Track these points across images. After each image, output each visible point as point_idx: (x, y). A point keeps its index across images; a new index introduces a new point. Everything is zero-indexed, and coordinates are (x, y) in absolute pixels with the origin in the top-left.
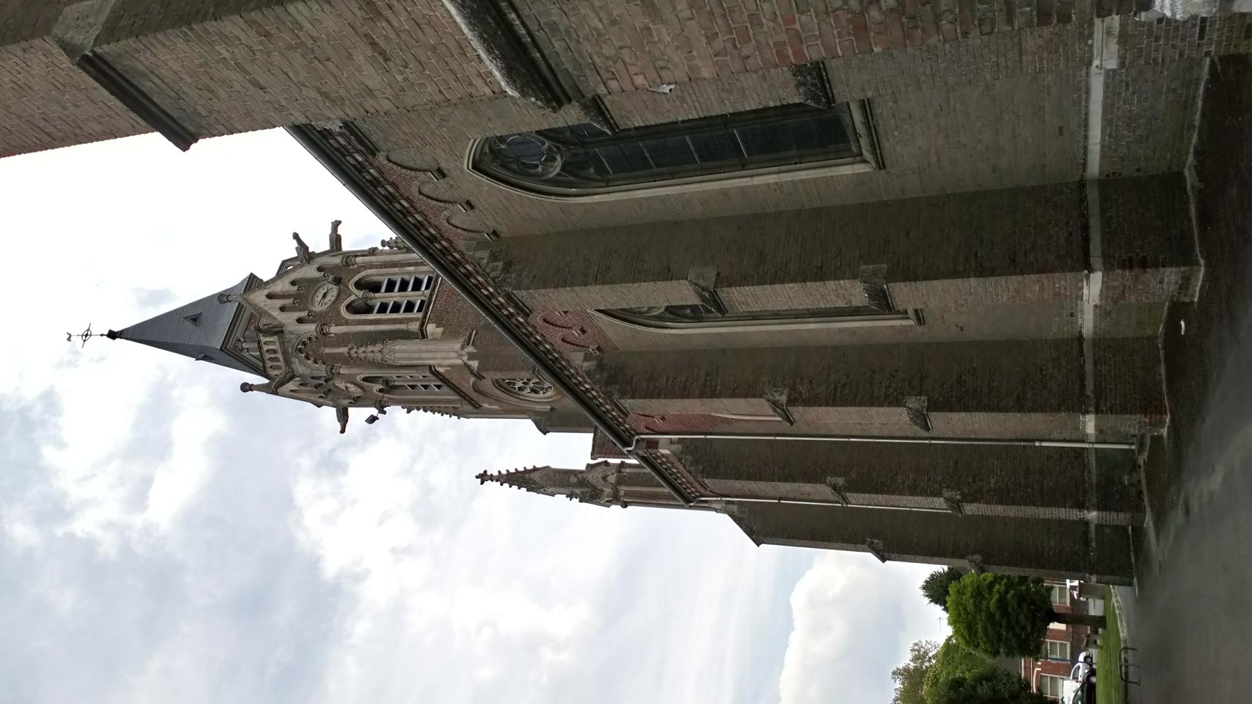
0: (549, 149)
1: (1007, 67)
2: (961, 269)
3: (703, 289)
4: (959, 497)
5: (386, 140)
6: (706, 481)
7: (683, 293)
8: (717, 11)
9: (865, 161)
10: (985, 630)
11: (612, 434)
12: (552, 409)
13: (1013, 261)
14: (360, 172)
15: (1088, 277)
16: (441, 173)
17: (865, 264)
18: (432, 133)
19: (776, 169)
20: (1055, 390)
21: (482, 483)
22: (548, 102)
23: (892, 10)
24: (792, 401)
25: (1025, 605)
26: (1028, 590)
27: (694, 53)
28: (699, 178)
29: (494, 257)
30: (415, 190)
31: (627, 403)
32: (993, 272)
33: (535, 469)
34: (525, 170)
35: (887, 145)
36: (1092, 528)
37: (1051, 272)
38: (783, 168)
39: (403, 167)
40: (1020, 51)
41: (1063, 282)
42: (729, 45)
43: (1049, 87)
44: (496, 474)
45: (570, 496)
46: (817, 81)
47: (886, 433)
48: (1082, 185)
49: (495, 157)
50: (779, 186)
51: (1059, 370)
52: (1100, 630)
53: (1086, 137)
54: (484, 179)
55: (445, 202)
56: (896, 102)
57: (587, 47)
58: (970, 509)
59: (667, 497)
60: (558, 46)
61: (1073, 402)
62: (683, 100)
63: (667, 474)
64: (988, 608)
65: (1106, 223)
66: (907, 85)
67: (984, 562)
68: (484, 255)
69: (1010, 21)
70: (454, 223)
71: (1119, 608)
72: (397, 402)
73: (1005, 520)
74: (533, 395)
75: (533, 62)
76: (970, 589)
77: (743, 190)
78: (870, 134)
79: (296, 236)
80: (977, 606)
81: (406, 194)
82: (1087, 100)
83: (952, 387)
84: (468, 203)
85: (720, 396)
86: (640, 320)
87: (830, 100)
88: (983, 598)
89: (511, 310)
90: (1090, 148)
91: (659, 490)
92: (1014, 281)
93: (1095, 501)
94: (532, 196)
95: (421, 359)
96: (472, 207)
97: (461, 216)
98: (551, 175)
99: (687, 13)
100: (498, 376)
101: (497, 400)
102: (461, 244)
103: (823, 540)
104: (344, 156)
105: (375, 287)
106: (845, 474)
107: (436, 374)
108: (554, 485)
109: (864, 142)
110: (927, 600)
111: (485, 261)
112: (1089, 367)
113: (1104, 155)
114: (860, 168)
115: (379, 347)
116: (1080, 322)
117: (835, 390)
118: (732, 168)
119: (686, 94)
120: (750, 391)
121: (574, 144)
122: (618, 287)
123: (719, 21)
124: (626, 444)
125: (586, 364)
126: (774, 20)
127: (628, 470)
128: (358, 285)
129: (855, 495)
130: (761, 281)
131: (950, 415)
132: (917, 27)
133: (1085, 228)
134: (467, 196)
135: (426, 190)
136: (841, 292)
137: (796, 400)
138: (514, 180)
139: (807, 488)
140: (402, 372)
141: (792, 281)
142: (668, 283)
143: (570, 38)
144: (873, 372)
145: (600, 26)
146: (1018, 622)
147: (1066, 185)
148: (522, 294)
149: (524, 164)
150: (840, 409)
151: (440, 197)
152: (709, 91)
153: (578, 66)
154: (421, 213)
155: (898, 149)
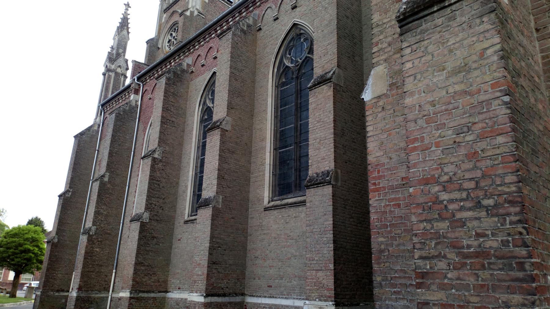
0: (297, 62)
1: (311, 264)
2: (214, 240)
3: (221, 123)
4: (91, 233)
6: (114, 115)
7: (220, 112)
8: (451, 106)
9: (269, 202)
10: (15, 242)
11: (145, 74)
12: (159, 48)
13: (214, 263)
15: (202, 295)
16: (294, 7)
19: (272, 164)
20: (144, 280)
21: (125, 4)
22: (404, 14)
23: (437, 198)
24: (154, 159)
25: (25, 261)
26: (33, 263)
27: (423, 94)
29: (249, 26)
31: (163, 80)
32: (210, 254)
33: (128, 33)
34: (289, 49)
35: (275, 212)
36: (66, 294)
37: (207, 279)
40: (318, 270)
41: (201, 284)
42: (426, 113)
43: (291, 282)
44: (128, 12)
45: (112, 48)
48: (243, 294)
49: (298, 35)
50: (263, 164)
51: (153, 282)
52: (8, 295)
53: (265, 297)
54: (288, 28)
55: (279, 7)
56: (295, 217)
57: (436, 36)
58: (83, 239)
59: (106, 96)
60: (439, 21)
61: (137, 287)
62: (318, 122)
63: (119, 97)
64: (26, 244)
65: (224, 304)
66: (309, 220)
67: (53, 244)
68: (251, 22)
69: (421, 258)
71: (20, 304)
73: (74, 254)
74: (167, 40)
75: (432, 6)
76: (37, 236)
77: (265, 148)
80: (27, 239)
82: (282, 298)
83: (152, 233)
84: (277, 19)
85: (161, 126)
86: (205, 94)
87: (308, 187)
88: (31, 243)
89: (219, 32)
90: (260, 298)
91: (110, 93)
92: (205, 263)
93: (82, 295)
96: (275, 20)
97: (271, 14)
98: (285, 61)
99: (451, 90)
100: (180, 24)
101: (167, 22)
102: (257, 12)
103: (74, 168)
106: (109, 182)
108: (119, 40)
109: (278, 203)
110: (30, 219)
111: (248, 21)
112: (152, 295)
113: (255, 304)
114: (266, 200)
116: (175, 292)
117: (157, 181)
118: (275, 144)
120: (162, 141)
121: (298, 74)
122: (227, 83)
123: (443, 108)
124: (139, 79)
125: (185, 64)
126: (440, 136)
127: (122, 79)
129: (98, 185)
130: (221, 150)
131: (138, 232)
132: (424, 210)
133: (224, 295)
134: (281, 18)
136: (210, 186)
137: (155, 162)
139: (104, 163)
141: (219, 164)
142: (226, 107)
143: (444, 27)
144: (164, 199)
145: (449, 44)
146: (17, 257)
147: (244, 288)
148: (229, 35)
149: (292, 49)
150: (148, 181)
152: (322, 134)
153: (423, 32)
155: (272, 217)
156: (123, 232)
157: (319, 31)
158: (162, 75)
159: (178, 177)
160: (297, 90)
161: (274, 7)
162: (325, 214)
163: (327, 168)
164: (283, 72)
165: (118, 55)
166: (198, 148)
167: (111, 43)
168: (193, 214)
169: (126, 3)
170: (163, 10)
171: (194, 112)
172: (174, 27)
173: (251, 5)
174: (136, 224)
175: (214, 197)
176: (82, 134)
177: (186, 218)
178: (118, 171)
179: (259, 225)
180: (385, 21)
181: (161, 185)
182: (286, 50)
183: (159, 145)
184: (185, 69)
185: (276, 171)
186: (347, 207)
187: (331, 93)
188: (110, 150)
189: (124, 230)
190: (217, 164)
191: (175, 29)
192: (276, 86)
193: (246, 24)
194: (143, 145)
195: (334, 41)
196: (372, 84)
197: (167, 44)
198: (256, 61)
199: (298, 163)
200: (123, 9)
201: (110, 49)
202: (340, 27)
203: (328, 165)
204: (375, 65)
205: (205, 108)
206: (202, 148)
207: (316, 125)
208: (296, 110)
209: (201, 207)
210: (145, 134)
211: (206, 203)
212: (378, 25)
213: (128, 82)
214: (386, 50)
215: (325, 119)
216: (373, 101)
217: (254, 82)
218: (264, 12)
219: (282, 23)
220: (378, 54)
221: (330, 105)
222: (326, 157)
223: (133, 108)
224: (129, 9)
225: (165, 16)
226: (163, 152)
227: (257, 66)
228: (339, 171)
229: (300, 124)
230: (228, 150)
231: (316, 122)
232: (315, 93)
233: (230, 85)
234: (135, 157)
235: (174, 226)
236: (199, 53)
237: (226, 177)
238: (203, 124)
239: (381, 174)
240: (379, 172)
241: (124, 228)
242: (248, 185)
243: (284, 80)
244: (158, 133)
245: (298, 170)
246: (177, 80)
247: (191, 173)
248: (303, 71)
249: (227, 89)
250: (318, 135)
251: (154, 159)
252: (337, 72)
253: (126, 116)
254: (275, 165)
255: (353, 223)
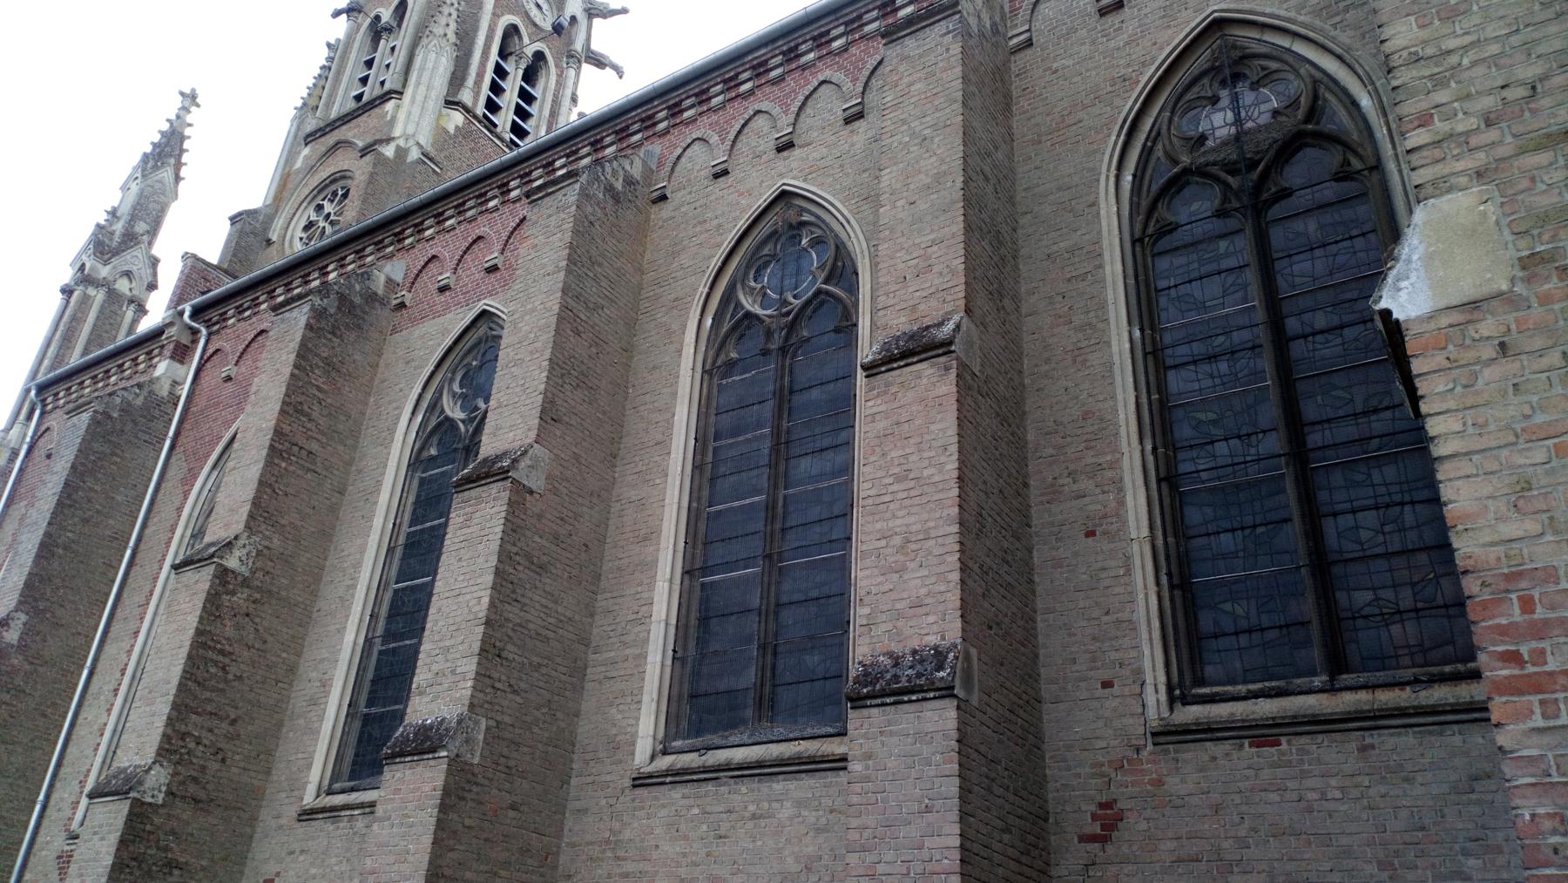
0: (785, 303)
3: (515, 461)
5: (904, 58)
9: (653, 758)
12: (269, 242)
14: (814, 39)
16: (785, 146)
17: (488, 729)
18: (904, 122)
19: (674, 621)
21: (182, 94)
24: (223, 574)
28: (685, 504)
29: (629, 182)
30: (764, 106)
31: (299, 316)
33: (178, 178)
34: (755, 264)
35: (677, 793)
38: (672, 631)
39: (807, 98)
44: (189, 119)
45: (113, 213)
46: (904, 683)
47: (80, 730)
49: (791, 227)
50: (643, 620)
55: (734, 142)
56: (754, 817)
59: (59, 360)
62: (899, 479)
63: (111, 365)
68: (636, 170)
70: (693, 152)
72: (350, 37)
74: (303, 223)
78: (706, 770)
79: (624, 11)
81: (758, 93)
83: (166, 849)
84: (725, 172)
85: (269, 463)
94: (715, 262)
95: (418, 84)
96: (716, 176)
97: (700, 161)
101: (311, 169)
102: (656, 147)
104: (846, 24)
105: (530, 76)
106: (22, 647)
107: (385, 97)
108: (141, 195)
111: (628, 167)
115: (452, 37)
117: (222, 652)
119: (912, 484)
120: (261, 512)
121: (787, 338)
124: (197, 312)
125: (382, 279)
127: (129, 315)
128: (539, 56)
130: (504, 556)
131: (113, 839)
135: (760, 121)
137: (224, 583)
138: (755, 232)
140: (402, 55)
141: (492, 604)
142: (536, 412)
148: (571, 194)
151: (741, 137)
152: (912, 519)
154: (723, 106)
155: (664, 812)
156: (40, 839)
157: (900, 203)
158: (300, 297)
159: (296, 645)
160: (782, 388)
161: (714, 139)
162: (928, 809)
163: (933, 640)
164: (733, 329)
165: (130, 239)
166: (391, 550)
168: (337, 786)
169: (188, 91)
170: (302, 134)
171: (392, 431)
172: (333, 188)
173: (636, 127)
174: (112, 807)
175: (459, 722)
177: (309, 799)
178: (59, 612)
179: (607, 842)
180: (1451, 44)
181: (233, 669)
182: (748, 267)
183: (248, 527)
184: (380, 292)
185: (685, 648)
186: (997, 790)
187: (947, 387)
188: (47, 534)
189: (42, 831)
190: (486, 601)
191: (335, 194)
192: (704, 371)
193: (621, 173)
194: (173, 531)
195: (953, 236)
196: (1428, 259)
197: (299, 233)
198: (640, 287)
199: (772, 625)
200: (173, 106)
201: (105, 216)
202: (971, 202)
203: (935, 628)
204: (1429, 190)
205: (433, 423)
206: (418, 551)
207: (891, 489)
208: (775, 449)
209: (402, 754)
210: (186, 495)
211: (425, 743)
212: (1417, 59)
213: (146, 325)
214: (1474, 141)
215: (926, 472)
216: (1444, 321)
217: (628, 350)
218: (679, 151)
219: (742, 188)
220: (1437, 153)
221: (945, 427)
222: (929, 600)
223: (160, 403)
224: (193, 109)
225: (306, 151)
226: (259, 553)
227: (644, 305)
228: (974, 652)
229: (785, 497)
230: (529, 557)
231: (891, 480)
232: (888, 385)
233: (557, 346)
234: (135, 569)
235: (253, 827)
236: (433, 252)
237: (511, 651)
238: (418, 474)
239: (1540, 613)
240: (1527, 605)
241: (45, 822)
242: (579, 689)
243: (734, 355)
244: (254, 485)
245: (770, 651)
246: (346, 325)
247: (349, 637)
248: (805, 333)
249: (547, 354)
250: (898, 522)
251: (223, 574)
252: (964, 328)
253: (129, 426)
254: (682, 628)
255: (1010, 851)
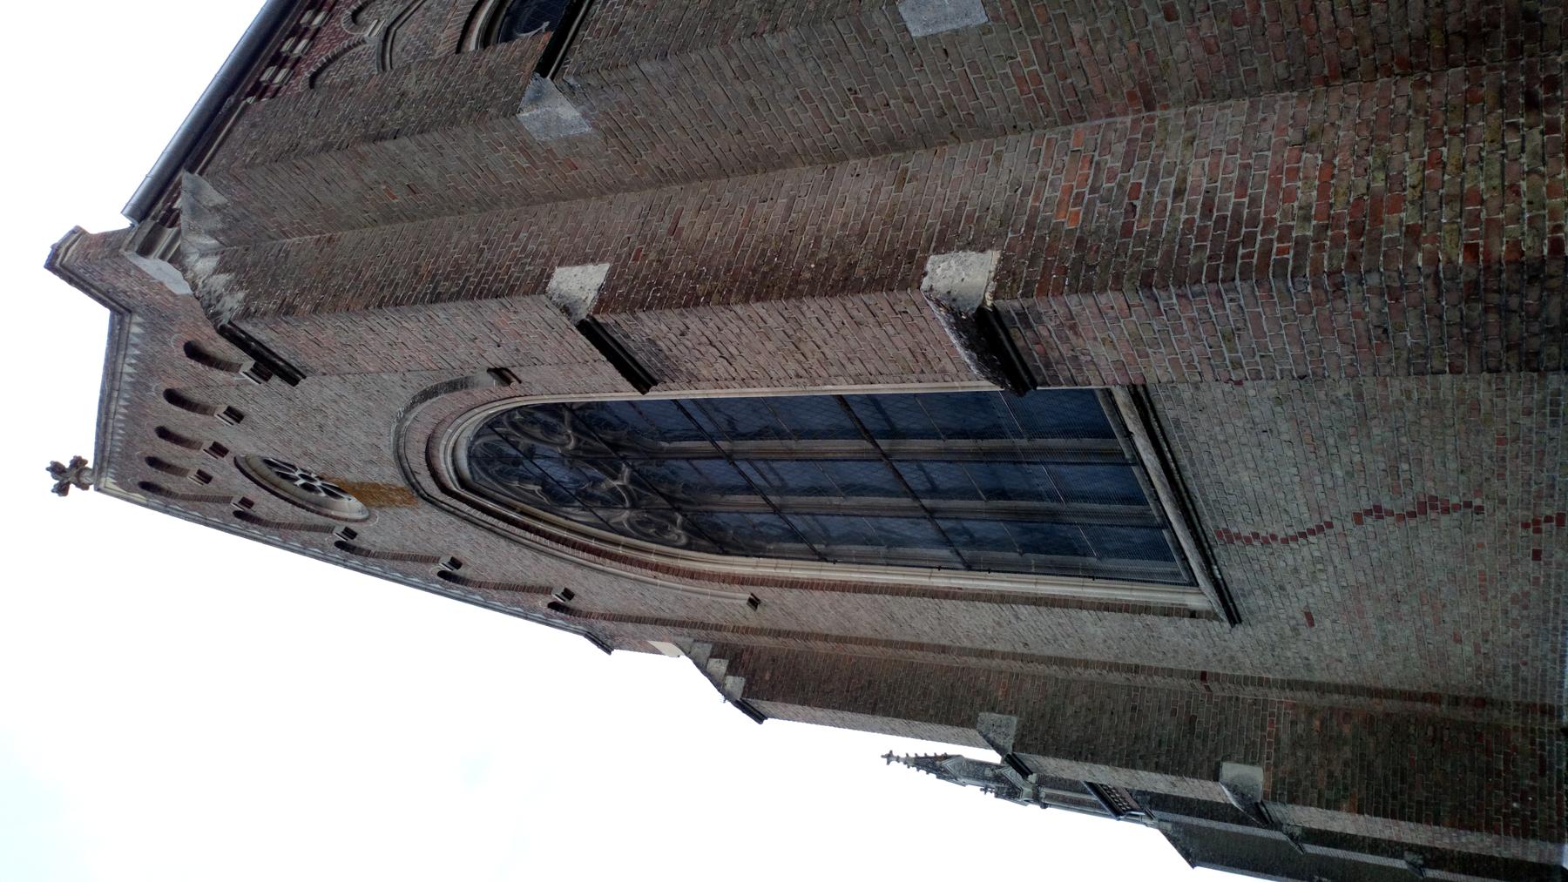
45: (985, 790)
59: (1100, 808)
108: (968, 777)
167: (973, 791)
176: (1187, 855)
